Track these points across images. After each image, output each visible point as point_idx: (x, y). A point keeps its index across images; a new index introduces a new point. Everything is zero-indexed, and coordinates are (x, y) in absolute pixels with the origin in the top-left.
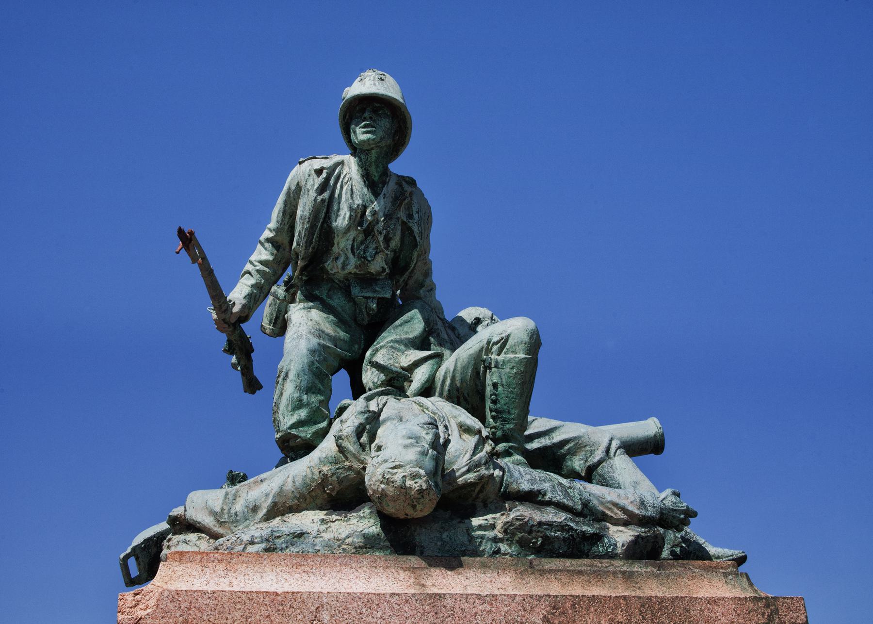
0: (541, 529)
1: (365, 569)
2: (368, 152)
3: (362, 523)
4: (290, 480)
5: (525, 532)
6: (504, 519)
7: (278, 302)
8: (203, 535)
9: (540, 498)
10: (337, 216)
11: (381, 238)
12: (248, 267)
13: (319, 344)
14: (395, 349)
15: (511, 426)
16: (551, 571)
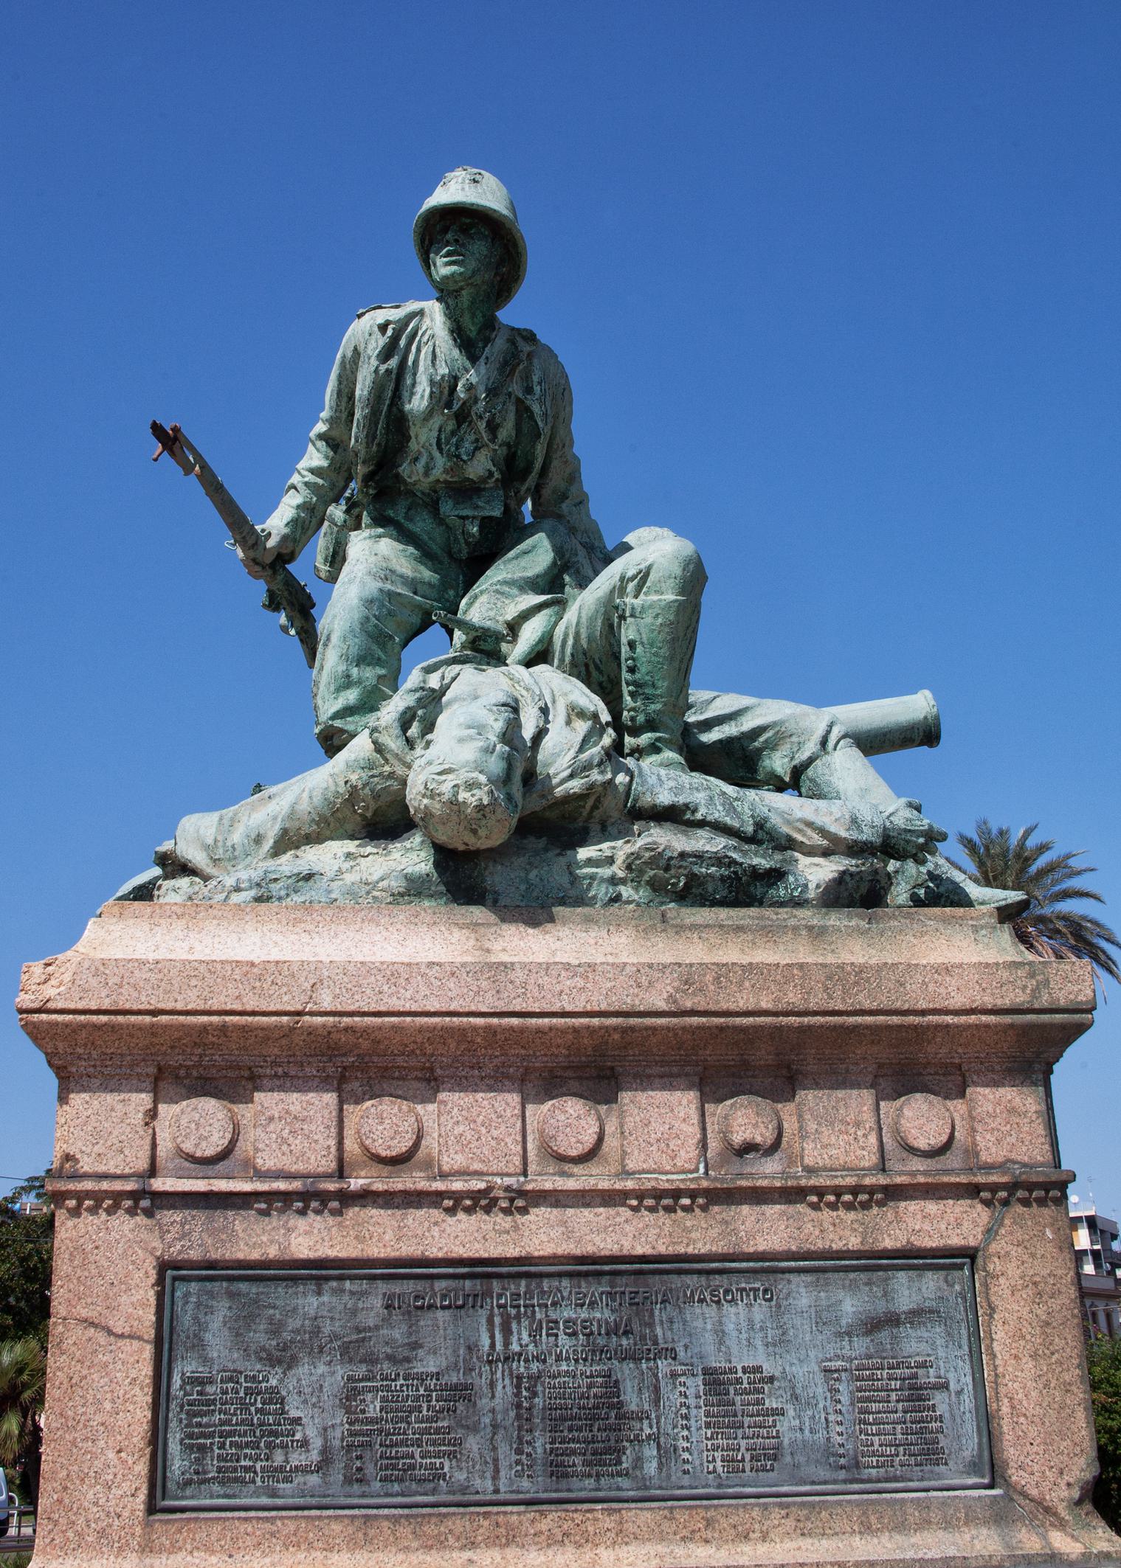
0: (684, 864)
1: (399, 926)
2: (456, 293)
3: (411, 857)
4: (305, 795)
5: (658, 868)
6: (629, 849)
7: (336, 529)
8: (197, 880)
9: (688, 816)
10: (412, 394)
11: (482, 425)
12: (295, 479)
13: (381, 590)
14: (502, 594)
15: (658, 706)
16: (693, 927)
